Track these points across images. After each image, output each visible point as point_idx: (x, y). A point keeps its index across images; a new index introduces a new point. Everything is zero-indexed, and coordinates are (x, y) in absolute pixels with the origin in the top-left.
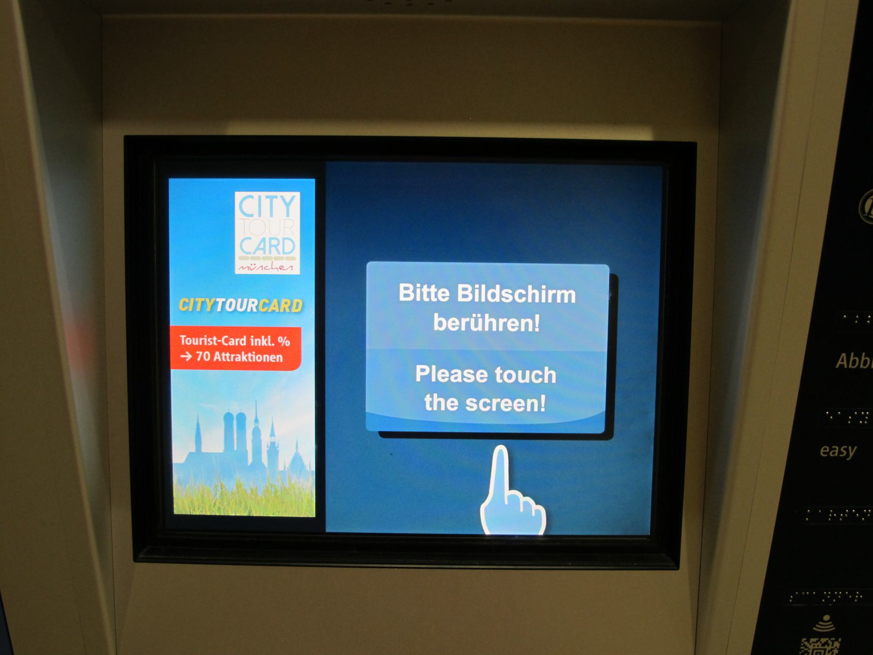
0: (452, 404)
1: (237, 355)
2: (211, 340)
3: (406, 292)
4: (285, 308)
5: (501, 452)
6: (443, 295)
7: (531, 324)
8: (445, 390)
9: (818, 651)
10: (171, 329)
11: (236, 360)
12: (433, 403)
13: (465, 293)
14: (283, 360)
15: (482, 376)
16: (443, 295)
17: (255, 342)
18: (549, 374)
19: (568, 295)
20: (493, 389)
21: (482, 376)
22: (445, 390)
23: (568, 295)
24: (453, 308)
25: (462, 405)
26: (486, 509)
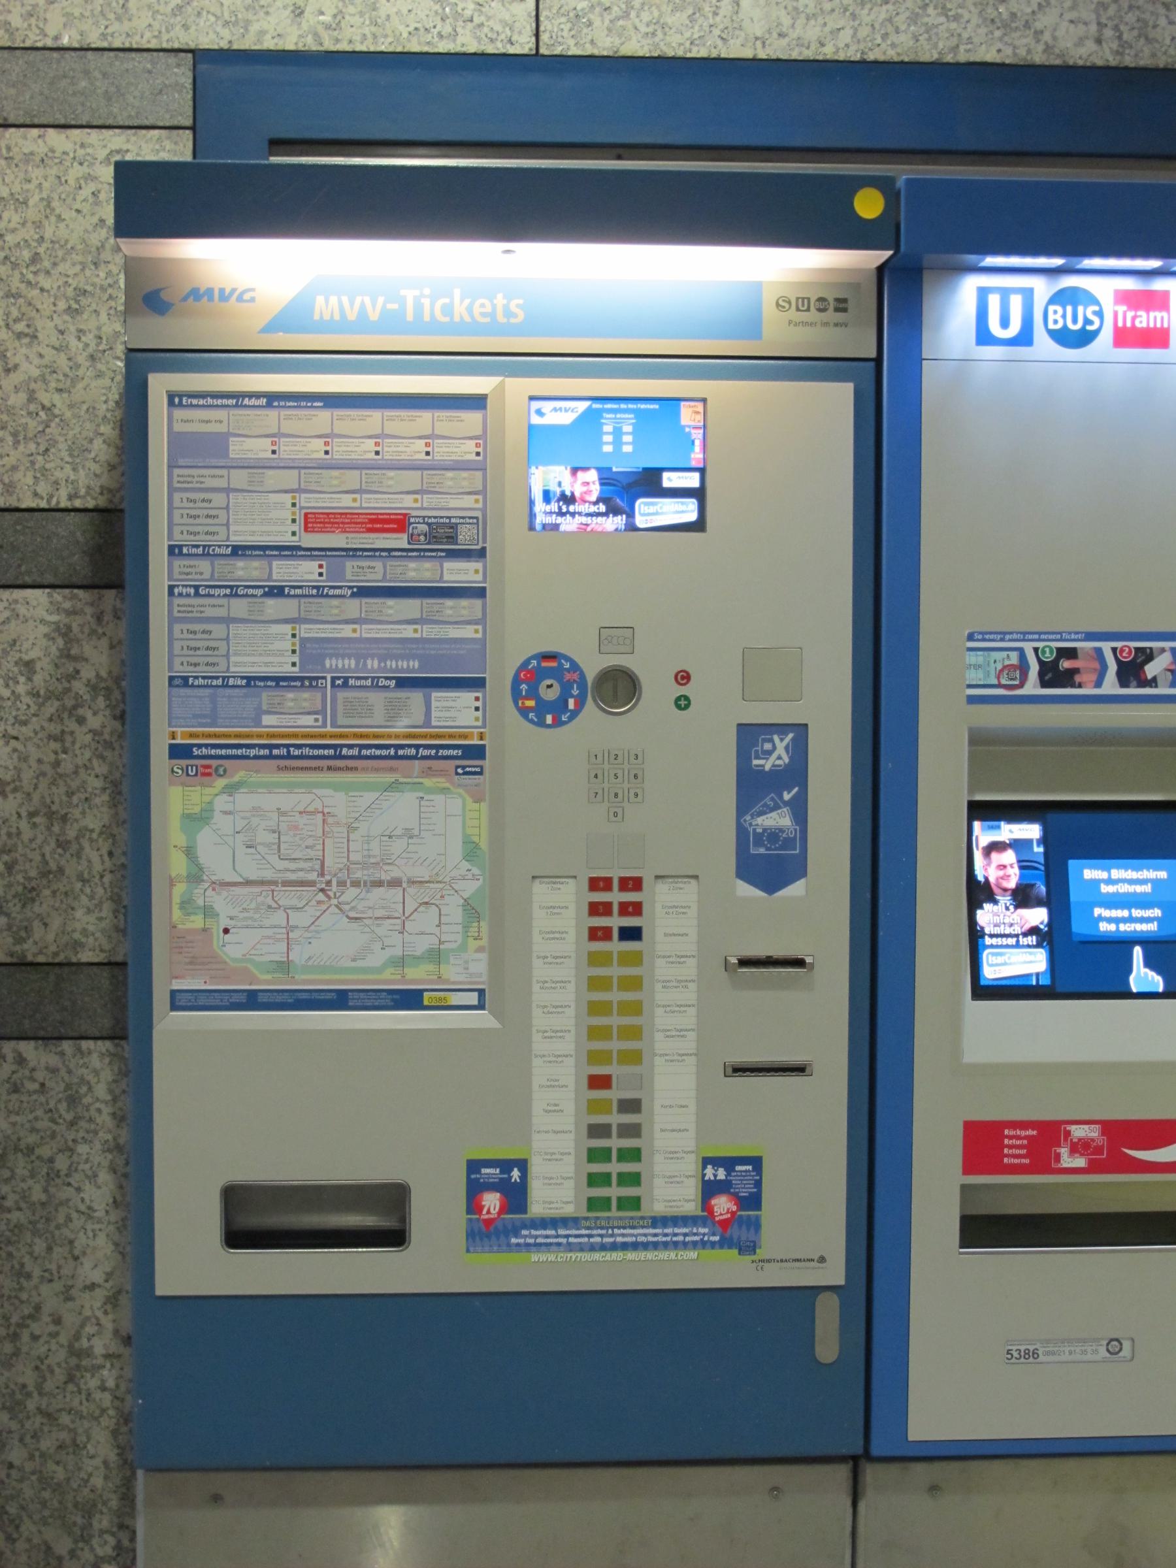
0: (1112, 927)
1: (1139, 313)
2: (516, 316)
3: (1088, 874)
4: (687, 1130)
5: (1138, 952)
6: (1104, 875)
7: (1147, 888)
8: (1110, 920)
9: (309, 511)
10: (1072, 906)
11: (1138, 324)
12: (1104, 927)
13: (1116, 874)
14: (794, 788)
15: (1125, 913)
16: (1104, 875)
17: (413, 751)
18: (1157, 912)
19: (1163, 875)
20: (1131, 919)
21: (1125, 913)
22: (1110, 920)
23: (1163, 875)
24: (1110, 881)
25: (1118, 928)
26: (1134, 979)
